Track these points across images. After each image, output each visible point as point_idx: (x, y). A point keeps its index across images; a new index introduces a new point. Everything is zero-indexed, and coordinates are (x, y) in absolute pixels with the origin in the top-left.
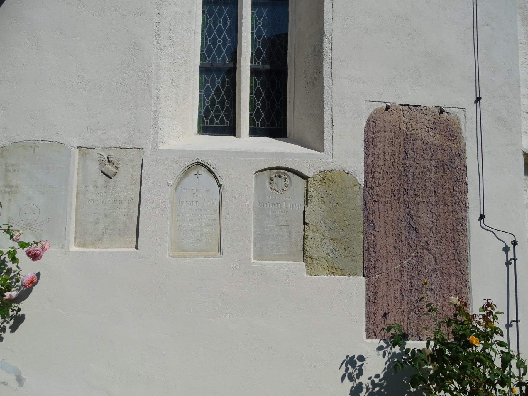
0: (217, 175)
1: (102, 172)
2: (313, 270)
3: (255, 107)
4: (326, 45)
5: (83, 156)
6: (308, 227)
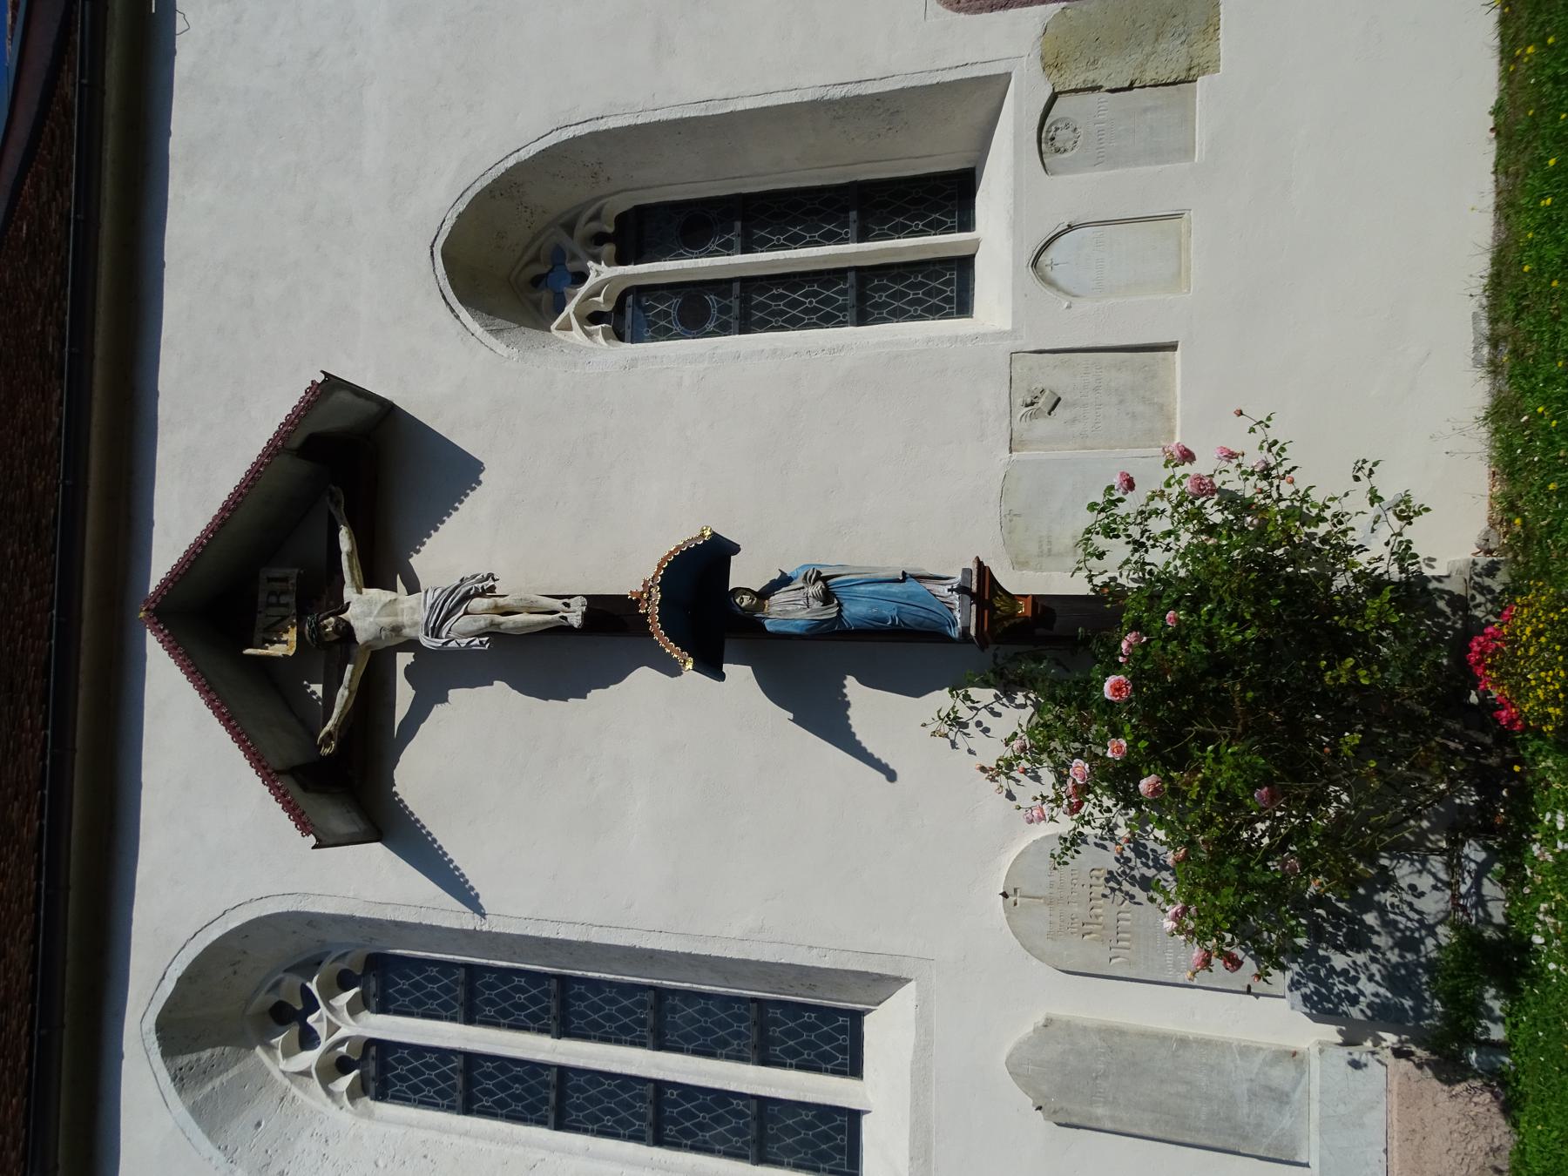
0: (1052, 234)
1: (1049, 413)
2: (1210, 64)
3: (921, 231)
4: (838, 93)
5: (1024, 444)
6: (1138, 82)
